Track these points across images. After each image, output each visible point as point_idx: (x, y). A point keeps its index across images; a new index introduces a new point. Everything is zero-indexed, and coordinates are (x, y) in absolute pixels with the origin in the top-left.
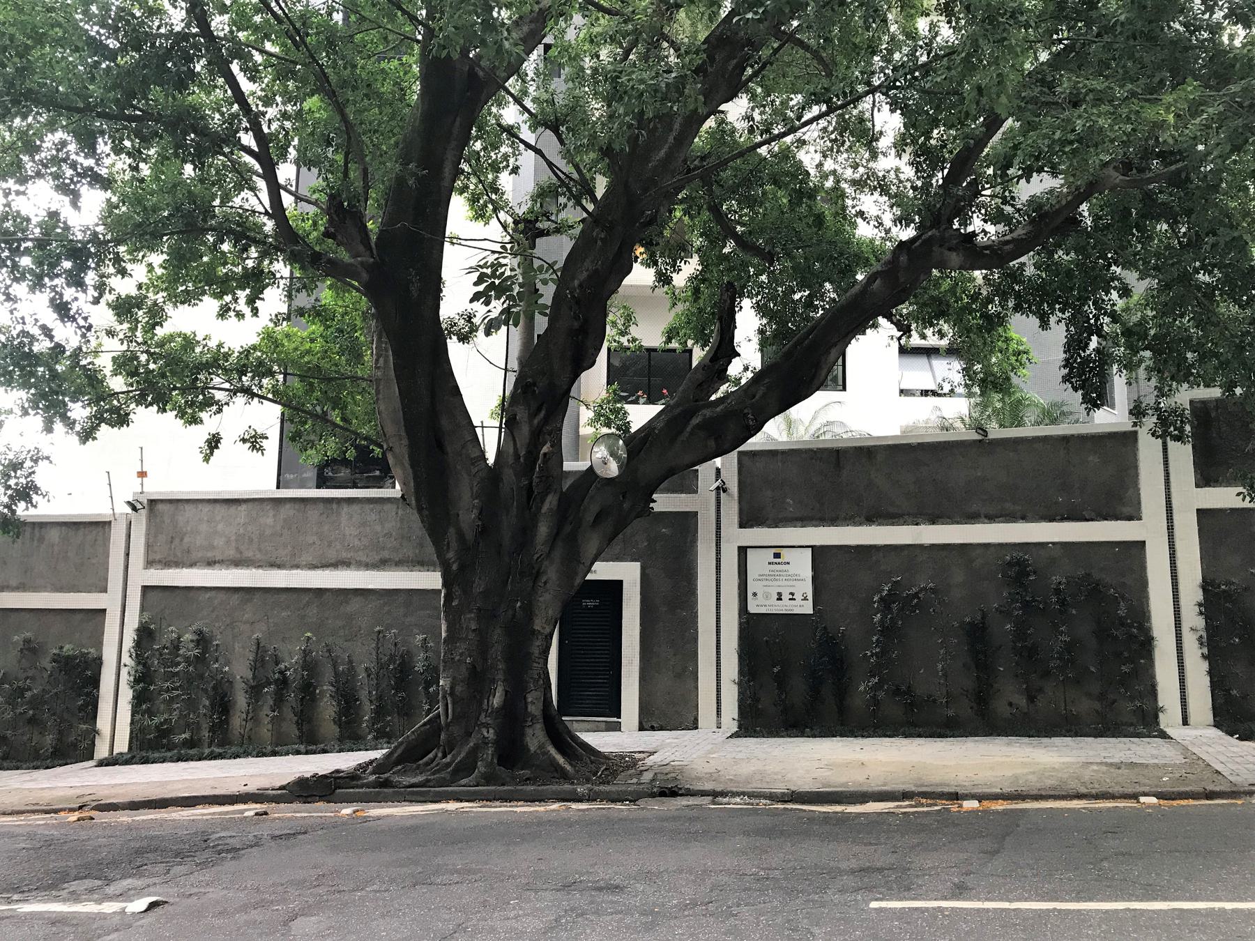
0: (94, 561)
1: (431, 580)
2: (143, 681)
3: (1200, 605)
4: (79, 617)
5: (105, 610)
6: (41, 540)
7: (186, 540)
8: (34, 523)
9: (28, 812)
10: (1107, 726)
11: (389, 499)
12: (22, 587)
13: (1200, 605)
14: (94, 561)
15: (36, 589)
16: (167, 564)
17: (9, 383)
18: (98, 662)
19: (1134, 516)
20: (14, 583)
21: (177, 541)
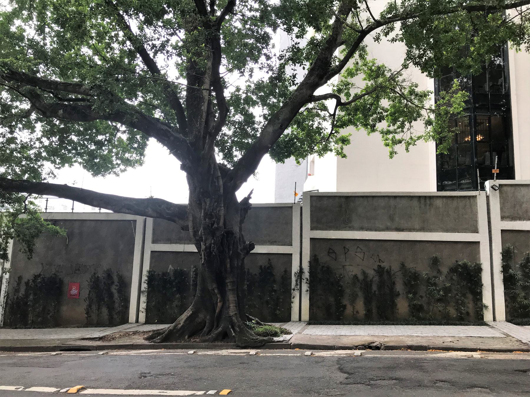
0: (465, 216)
1: (192, 248)
2: (509, 281)
3: (502, 272)
4: (460, 246)
5: (479, 242)
6: (431, 205)
7: (524, 205)
8: (425, 197)
9: (519, 350)
10: (461, 320)
11: (455, 196)
12: (422, 229)
13: (502, 272)
14: (465, 216)
15: (430, 230)
16: (513, 218)
17: (1, 166)
18: (479, 270)
19: (476, 231)
20: (417, 227)
21: (518, 207)
